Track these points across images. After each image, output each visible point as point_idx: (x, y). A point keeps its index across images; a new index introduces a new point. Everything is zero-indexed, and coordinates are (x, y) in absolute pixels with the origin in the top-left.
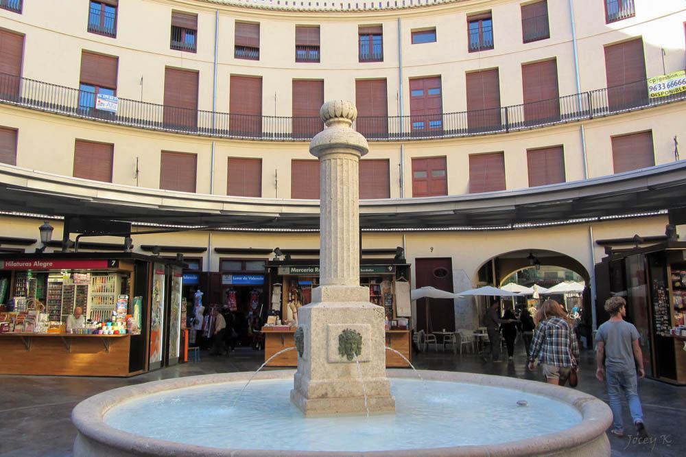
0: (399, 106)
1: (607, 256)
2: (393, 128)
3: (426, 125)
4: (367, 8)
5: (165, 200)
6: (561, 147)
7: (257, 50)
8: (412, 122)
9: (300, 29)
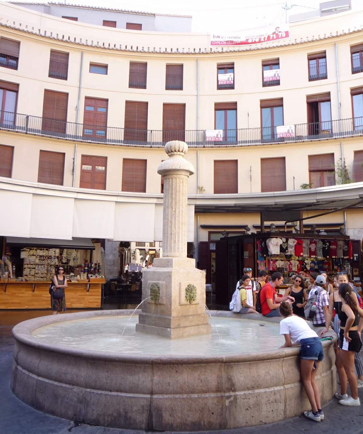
0: (75, 115)
2: (70, 130)
3: (94, 133)
7: (17, 59)
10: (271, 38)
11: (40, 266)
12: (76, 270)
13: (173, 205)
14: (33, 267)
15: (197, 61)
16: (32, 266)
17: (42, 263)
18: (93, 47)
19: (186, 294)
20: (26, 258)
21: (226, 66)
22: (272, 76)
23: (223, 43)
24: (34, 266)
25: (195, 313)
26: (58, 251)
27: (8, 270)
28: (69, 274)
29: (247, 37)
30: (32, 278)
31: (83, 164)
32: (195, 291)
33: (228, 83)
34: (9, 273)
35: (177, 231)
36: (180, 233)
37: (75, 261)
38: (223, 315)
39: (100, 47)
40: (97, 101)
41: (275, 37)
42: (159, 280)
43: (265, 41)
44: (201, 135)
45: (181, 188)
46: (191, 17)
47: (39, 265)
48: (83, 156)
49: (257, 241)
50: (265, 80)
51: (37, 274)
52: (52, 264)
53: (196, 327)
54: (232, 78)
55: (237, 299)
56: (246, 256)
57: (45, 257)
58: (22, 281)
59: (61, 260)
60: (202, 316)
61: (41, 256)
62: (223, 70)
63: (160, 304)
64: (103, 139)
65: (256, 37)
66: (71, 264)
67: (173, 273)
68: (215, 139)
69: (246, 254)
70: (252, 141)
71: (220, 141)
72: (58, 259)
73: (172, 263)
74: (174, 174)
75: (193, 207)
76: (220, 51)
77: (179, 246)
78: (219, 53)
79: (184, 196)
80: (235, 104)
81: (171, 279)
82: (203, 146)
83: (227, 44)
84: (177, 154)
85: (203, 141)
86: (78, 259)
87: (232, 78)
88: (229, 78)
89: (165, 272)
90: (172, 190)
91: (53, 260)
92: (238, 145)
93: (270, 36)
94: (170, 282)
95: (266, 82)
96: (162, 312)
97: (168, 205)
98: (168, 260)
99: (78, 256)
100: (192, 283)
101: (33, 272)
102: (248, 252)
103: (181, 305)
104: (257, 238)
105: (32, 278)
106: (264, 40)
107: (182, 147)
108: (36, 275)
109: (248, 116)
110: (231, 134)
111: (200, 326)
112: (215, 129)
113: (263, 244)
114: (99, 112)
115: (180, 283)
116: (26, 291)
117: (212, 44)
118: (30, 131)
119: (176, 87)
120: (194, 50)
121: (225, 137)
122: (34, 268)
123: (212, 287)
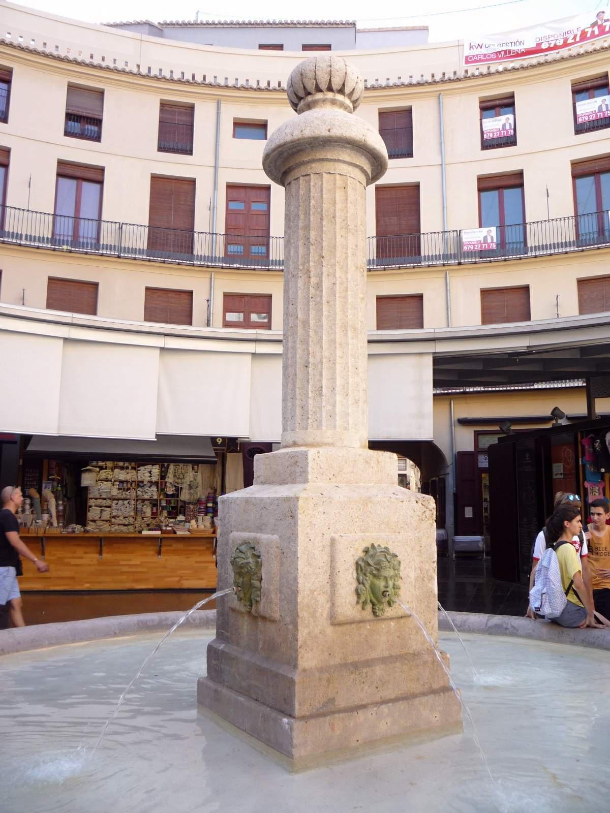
1: (156, 440)
2: (201, 247)
3: (247, 252)
4: (152, 74)
5: (168, 339)
6: (420, 297)
7: (98, 122)
8: (227, 243)
9: (165, 106)
10: (589, 35)
11: (120, 502)
12: (190, 508)
13: (311, 264)
14: (107, 504)
15: (439, 98)
16: (104, 503)
17: (124, 496)
18: (238, 89)
19: (358, 580)
20: (92, 486)
21: (497, 102)
22: (594, 110)
23: (489, 56)
24: (108, 502)
25: (396, 652)
26: (156, 470)
27: (49, 512)
28: (175, 518)
29: (538, 40)
30: (106, 527)
31: (226, 310)
32: (392, 573)
33: (504, 133)
34: (51, 516)
35: (326, 353)
36: (338, 360)
37: (192, 491)
38: (507, 629)
39: (251, 88)
40: (249, 191)
41: (597, 32)
42: (260, 529)
43: (576, 43)
44: (452, 240)
45: (339, 206)
46: (426, 29)
47: (118, 500)
48: (226, 295)
49: (582, 438)
50: (580, 120)
51: (114, 517)
52: (146, 497)
53: (402, 705)
54: (510, 124)
55: (552, 578)
56: (556, 475)
57: (131, 484)
58: (74, 532)
59: (162, 490)
60: (425, 663)
61: (122, 482)
62: (493, 112)
63: (264, 618)
64: (93, 248)
65: (556, 36)
66: (185, 496)
67: (300, 503)
68: (481, 246)
69: (558, 469)
70: (558, 245)
71: (492, 251)
72: (157, 488)
73: (307, 466)
74: (313, 161)
75: (429, 360)
76: (485, 71)
77: (334, 406)
78: (482, 75)
79: (350, 236)
80: (520, 174)
81: (296, 524)
82: (457, 262)
83: (497, 59)
84: (324, 101)
85: (456, 252)
86: (197, 487)
87: (510, 124)
88: (504, 125)
89: (278, 499)
90: (307, 214)
91: (146, 488)
92: (529, 254)
93: (586, 30)
94: (292, 537)
95: (583, 124)
96: (271, 647)
97: (296, 268)
98: (292, 456)
99: (198, 481)
100: (382, 539)
101: (106, 514)
102: (561, 464)
103: (335, 622)
104: (582, 433)
105: (106, 527)
106: (573, 41)
107: (342, 74)
108: (113, 520)
109: (548, 196)
110: (513, 235)
111: (416, 701)
112: (480, 226)
113: (597, 445)
114: (253, 211)
115: (333, 541)
116: (86, 553)
117: (467, 62)
118: (125, 252)
119: (400, 153)
120: (433, 76)
121: (502, 243)
122: (109, 507)
123: (485, 541)
